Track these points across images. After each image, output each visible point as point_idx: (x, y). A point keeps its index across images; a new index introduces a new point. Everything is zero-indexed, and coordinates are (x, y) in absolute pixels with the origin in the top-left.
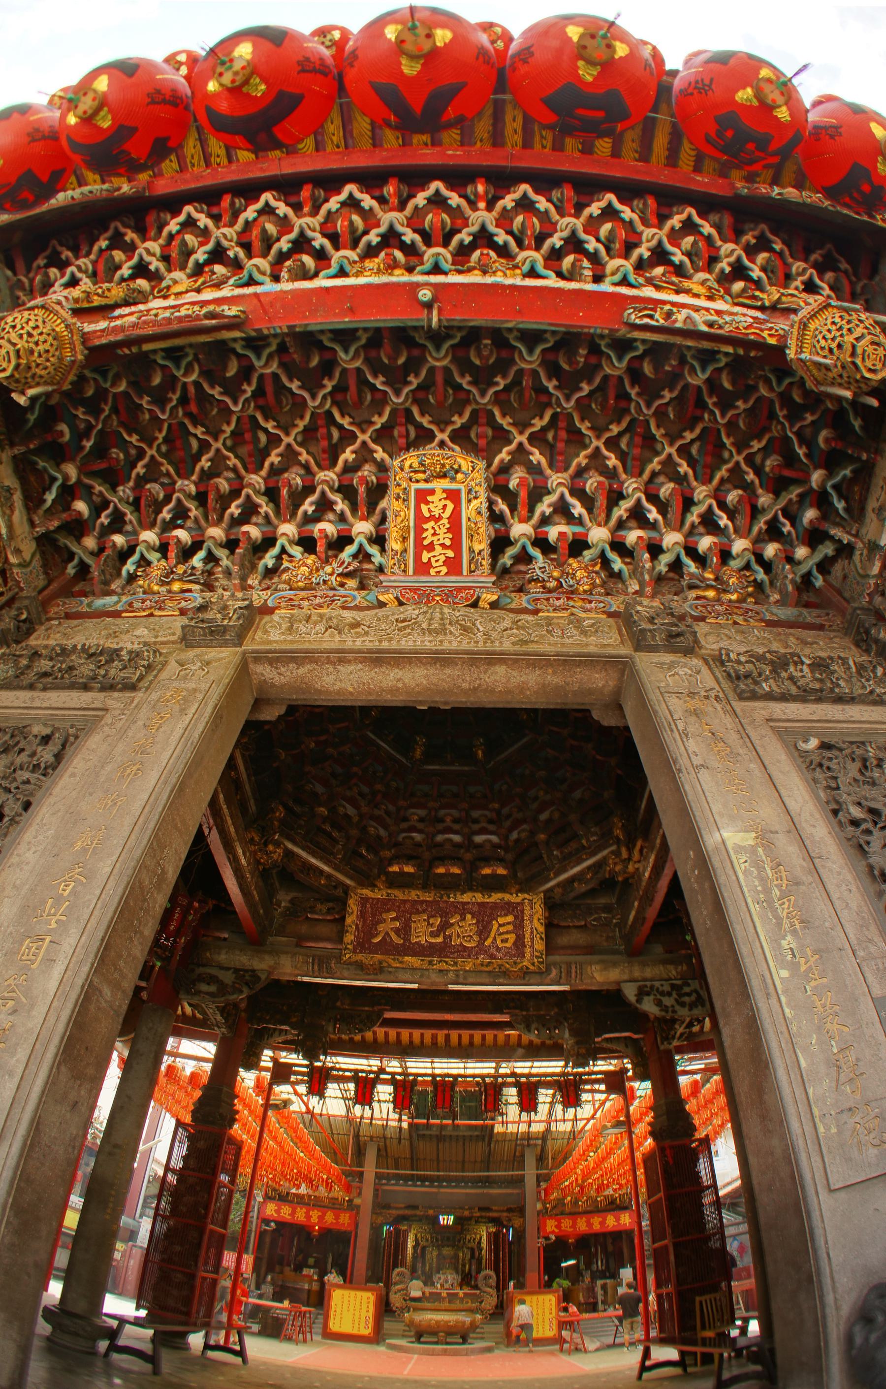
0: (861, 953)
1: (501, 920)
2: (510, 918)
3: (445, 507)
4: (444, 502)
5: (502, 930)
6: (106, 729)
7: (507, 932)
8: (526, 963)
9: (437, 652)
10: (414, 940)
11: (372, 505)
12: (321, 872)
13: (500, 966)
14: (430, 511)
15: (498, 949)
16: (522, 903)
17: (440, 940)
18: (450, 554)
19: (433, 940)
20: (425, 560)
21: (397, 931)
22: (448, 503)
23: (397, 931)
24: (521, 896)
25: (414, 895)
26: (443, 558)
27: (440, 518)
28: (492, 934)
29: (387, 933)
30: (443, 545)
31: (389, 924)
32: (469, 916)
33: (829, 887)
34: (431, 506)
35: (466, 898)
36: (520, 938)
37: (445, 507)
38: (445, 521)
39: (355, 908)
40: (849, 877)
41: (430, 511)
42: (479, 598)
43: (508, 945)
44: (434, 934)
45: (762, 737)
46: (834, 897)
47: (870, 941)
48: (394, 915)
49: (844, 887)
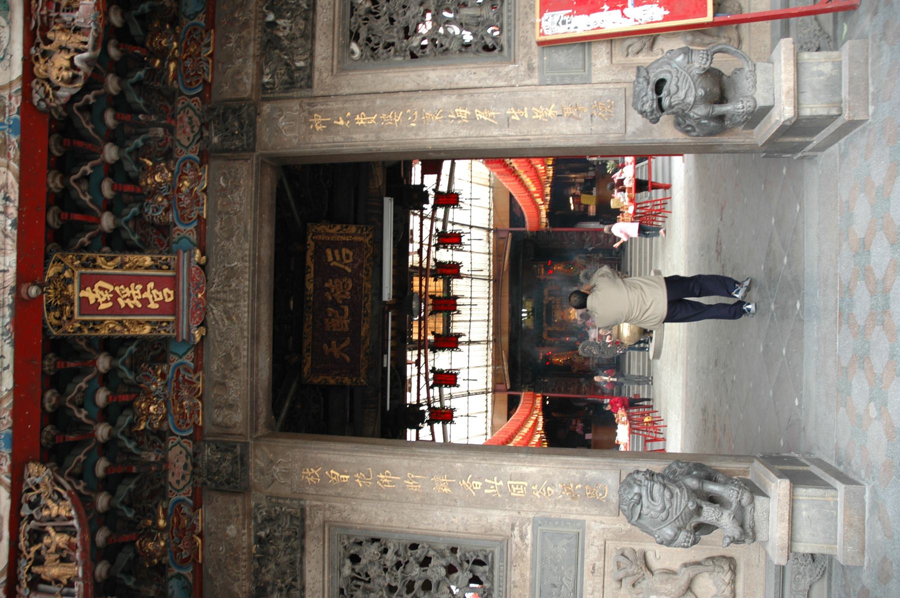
0: (513, 82)
1: (330, 258)
2: (329, 252)
3: (101, 288)
4: (96, 289)
5: (338, 258)
6: (345, 514)
7: (340, 254)
8: (367, 240)
9: (253, 296)
10: (347, 329)
11: (76, 354)
12: (291, 409)
13: (368, 261)
14: (106, 301)
15: (355, 261)
16: (316, 242)
17: (346, 309)
18: (151, 285)
19: (347, 314)
20: (157, 306)
21: (339, 343)
22: (97, 286)
23: (339, 343)
24: (309, 241)
25: (307, 330)
26: (155, 292)
27: (114, 292)
28: (342, 266)
29: (342, 350)
30: (143, 291)
31: (334, 349)
32: (326, 285)
33: (471, 85)
34: (100, 300)
35: (310, 287)
36: (346, 244)
37: (101, 288)
38: (117, 289)
39: (321, 378)
40: (466, 70)
41: (106, 301)
42: (198, 264)
43: (351, 254)
44: (342, 313)
45: (349, 85)
46: (477, 84)
47: (507, 74)
48: (325, 346)
49: (472, 76)
